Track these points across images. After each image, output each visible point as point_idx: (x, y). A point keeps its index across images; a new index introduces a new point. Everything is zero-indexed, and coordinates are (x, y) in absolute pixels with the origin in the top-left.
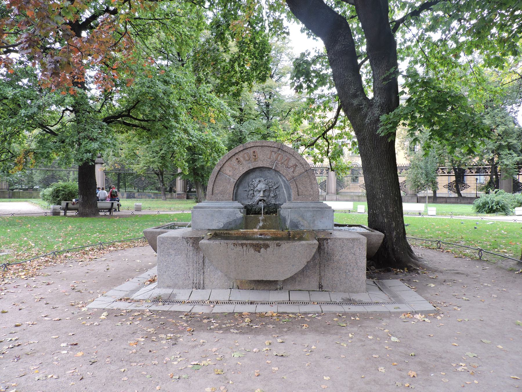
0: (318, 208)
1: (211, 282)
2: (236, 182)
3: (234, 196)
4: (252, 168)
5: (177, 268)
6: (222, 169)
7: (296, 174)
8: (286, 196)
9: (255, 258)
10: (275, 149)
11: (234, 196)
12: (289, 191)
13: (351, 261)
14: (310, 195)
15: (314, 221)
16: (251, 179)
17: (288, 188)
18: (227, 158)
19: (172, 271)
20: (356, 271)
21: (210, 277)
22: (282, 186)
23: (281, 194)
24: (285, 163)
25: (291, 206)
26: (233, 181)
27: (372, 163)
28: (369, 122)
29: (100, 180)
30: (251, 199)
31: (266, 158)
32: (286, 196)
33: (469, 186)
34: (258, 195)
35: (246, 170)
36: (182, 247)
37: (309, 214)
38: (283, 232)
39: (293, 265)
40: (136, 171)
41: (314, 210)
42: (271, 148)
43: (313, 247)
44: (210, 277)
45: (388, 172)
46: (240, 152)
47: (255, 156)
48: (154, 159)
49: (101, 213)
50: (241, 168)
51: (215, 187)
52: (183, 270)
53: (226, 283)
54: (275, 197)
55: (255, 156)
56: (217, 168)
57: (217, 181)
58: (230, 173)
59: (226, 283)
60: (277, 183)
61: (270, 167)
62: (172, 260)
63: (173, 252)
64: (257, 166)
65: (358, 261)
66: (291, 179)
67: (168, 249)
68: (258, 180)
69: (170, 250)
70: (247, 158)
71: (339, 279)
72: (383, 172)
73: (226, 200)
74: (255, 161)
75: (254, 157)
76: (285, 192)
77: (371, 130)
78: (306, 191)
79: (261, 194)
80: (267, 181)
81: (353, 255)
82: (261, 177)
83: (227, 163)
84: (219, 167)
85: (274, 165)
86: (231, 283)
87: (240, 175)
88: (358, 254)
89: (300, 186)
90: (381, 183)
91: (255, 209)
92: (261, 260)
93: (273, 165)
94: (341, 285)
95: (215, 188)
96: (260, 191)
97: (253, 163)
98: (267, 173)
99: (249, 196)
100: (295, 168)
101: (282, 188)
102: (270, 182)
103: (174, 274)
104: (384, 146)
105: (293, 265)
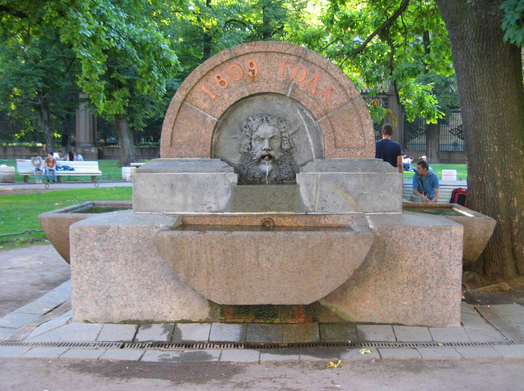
8: (313, 149)
10: (292, 58)
13: (435, 269)
31: (274, 76)
32: (313, 149)
35: (235, 98)
42: (284, 57)
50: (226, 95)
51: (176, 133)
56: (179, 96)
58: (206, 105)
61: (283, 93)
62: (98, 269)
65: (448, 269)
66: (322, 116)
69: (96, 252)
85: (290, 89)
88: (446, 256)
89: (339, 130)
92: (269, 266)
93: (288, 88)
94: (414, 313)
95: (177, 134)
97: (250, 86)
101: (305, 133)
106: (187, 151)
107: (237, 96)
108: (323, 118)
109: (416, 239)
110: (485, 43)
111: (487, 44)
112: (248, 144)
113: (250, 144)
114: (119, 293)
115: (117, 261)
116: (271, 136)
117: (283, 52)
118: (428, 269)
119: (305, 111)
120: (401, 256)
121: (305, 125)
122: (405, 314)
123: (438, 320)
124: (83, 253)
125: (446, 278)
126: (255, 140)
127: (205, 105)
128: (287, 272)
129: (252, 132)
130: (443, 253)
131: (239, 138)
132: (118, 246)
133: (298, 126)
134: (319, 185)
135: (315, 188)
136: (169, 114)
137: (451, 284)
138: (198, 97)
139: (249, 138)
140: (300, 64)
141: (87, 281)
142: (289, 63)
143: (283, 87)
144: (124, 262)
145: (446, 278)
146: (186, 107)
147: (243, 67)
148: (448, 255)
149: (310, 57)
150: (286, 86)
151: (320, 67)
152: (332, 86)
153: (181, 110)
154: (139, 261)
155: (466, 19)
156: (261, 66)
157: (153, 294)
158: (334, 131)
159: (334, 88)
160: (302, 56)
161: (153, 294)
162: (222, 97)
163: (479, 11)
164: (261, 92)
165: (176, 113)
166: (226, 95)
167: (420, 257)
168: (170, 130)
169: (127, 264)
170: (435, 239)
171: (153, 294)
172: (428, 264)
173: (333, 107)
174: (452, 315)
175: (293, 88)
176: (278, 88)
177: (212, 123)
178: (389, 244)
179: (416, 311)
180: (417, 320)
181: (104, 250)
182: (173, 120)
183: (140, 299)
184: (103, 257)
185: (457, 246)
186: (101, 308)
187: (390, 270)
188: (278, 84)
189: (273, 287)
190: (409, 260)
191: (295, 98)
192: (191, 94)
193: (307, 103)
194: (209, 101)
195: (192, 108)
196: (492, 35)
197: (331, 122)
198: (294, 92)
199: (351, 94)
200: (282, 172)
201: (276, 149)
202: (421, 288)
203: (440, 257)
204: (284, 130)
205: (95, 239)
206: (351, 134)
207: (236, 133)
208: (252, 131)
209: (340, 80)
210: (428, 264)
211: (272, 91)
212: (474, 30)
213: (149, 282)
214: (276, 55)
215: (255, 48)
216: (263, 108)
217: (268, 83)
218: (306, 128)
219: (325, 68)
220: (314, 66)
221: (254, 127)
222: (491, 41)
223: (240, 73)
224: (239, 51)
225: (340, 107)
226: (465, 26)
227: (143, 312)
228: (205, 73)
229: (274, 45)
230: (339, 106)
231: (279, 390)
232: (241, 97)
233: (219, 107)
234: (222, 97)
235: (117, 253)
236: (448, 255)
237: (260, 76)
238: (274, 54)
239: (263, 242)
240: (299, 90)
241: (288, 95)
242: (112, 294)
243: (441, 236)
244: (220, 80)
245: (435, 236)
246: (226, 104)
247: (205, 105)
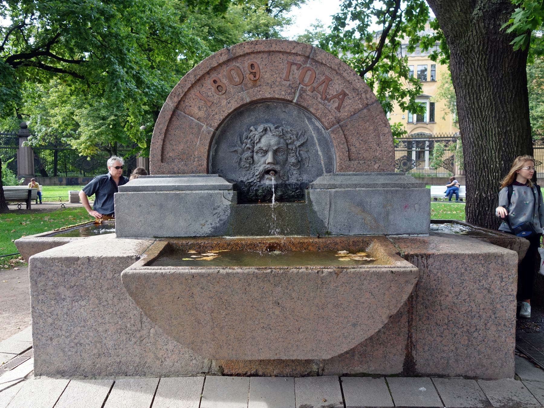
0: (396, 185)
1: (158, 359)
2: (214, 134)
3: (210, 164)
4: (248, 100)
5: (79, 329)
6: (183, 105)
7: (344, 114)
8: (322, 162)
9: (261, 309)
10: (299, 58)
11: (210, 164)
12: (329, 151)
13: (482, 306)
14: (376, 159)
15: (387, 215)
16: (245, 127)
17: (326, 144)
18: (192, 79)
19: (67, 337)
20: (493, 328)
21: (157, 349)
22: (313, 140)
23: (312, 159)
24: (321, 89)
25: (335, 182)
26: (207, 130)
27: (484, 98)
28: (481, 14)
29: (27, 160)
30: (248, 169)
31: (278, 79)
32: (322, 162)
33: (541, 163)
34: (263, 160)
35: (234, 105)
36: (89, 281)
37: (376, 201)
38: (320, 240)
39: (354, 325)
40: (76, 148)
41: (387, 192)
42: (290, 57)
43: (407, 282)
44: (157, 349)
45: (516, 116)
46: (220, 65)
47: (254, 74)
48: (99, 130)
49: (12, 207)
50: (224, 102)
51: (168, 145)
52: (91, 334)
53: (194, 361)
54: (300, 163)
55: (254, 74)
56: (170, 103)
57: (172, 132)
58: (201, 114)
59: (194, 361)
60: (303, 134)
61: (289, 98)
62: (65, 310)
63: (68, 293)
64: (259, 97)
65: (498, 306)
66: (333, 125)
67: (56, 286)
68: (260, 128)
69: (61, 289)
70: (237, 80)
71: (453, 348)
72: (505, 116)
73: (193, 172)
74: (254, 86)
75: (252, 76)
76: (320, 153)
77: (484, 31)
78: (367, 150)
79: (269, 158)
80: (280, 129)
81: (485, 292)
82: (267, 121)
83: (192, 92)
84: (176, 100)
85: (297, 94)
86: (206, 361)
87: (222, 118)
88: (497, 291)
89: (353, 140)
90: (500, 139)
91: (257, 190)
92: (277, 312)
93: (295, 93)
94: (457, 361)
95: (168, 146)
96: (266, 152)
97: (251, 91)
98: (281, 113)
99: (242, 163)
100: (342, 101)
101: (314, 145)
102: (287, 132)
103: (73, 344)
104: (509, 64)
105: (354, 325)
106: (180, 166)
107: (236, 103)
108: (335, 126)
109: (458, 269)
110: (493, 55)
111: (494, 57)
112: (249, 158)
113: (252, 157)
114: (90, 339)
115: (89, 300)
116: (275, 148)
117: (289, 51)
118: (474, 306)
119: (313, 120)
120: (440, 291)
121: (314, 135)
122: (446, 362)
123: (487, 370)
124: (45, 290)
125: (496, 318)
126: (257, 152)
127: (200, 113)
128: (302, 319)
129: (253, 145)
130: (492, 287)
131: (239, 152)
132: (89, 281)
133: (306, 136)
134: (333, 203)
135: (328, 206)
136: (159, 124)
137: (502, 325)
139: (250, 151)
140: (308, 65)
141: (51, 324)
142: (296, 64)
143: (289, 91)
144: (97, 302)
145: (496, 318)
146: (179, 116)
147: (242, 70)
148: (499, 289)
149: (319, 57)
150: (293, 91)
151: (331, 67)
152: (345, 90)
153: (173, 119)
154: (115, 300)
155: (472, 31)
156: (263, 68)
157: (133, 340)
158: (347, 142)
159: (347, 92)
160: (311, 56)
161: (133, 339)
162: (219, 104)
163: (487, 21)
164: (264, 97)
165: (166, 124)
166: (224, 102)
167: (464, 291)
168: (160, 142)
169: (100, 304)
170: (483, 269)
171: (133, 339)
172: (474, 300)
173: (346, 114)
174: (505, 364)
175: (300, 93)
176: (283, 93)
177: (209, 133)
178: (425, 276)
179: (460, 358)
180: (460, 369)
181: (71, 287)
182: (164, 130)
183: (117, 347)
184: (71, 295)
185: (510, 277)
186: (69, 359)
187: (426, 308)
188: (284, 88)
189: (282, 338)
190: (450, 295)
191: (303, 104)
192: (184, 101)
193: (317, 110)
194: (205, 109)
195: (185, 117)
196: (501, 47)
197: (343, 132)
198: (302, 98)
199: (367, 99)
200: (288, 189)
201: (282, 163)
202: (465, 330)
203: (489, 291)
204: (290, 141)
205: (60, 273)
206: (366, 145)
207: (235, 146)
208: (254, 143)
209: (353, 83)
210: (474, 300)
212: (480, 42)
213: (128, 325)
214: (281, 55)
215: (257, 47)
216: (266, 117)
218: (315, 139)
219: (337, 68)
220: (324, 67)
221: (255, 138)
222: (499, 53)
223: (239, 76)
224: (238, 50)
225: (354, 114)
226: (471, 38)
227: (120, 361)
228: (199, 76)
230: (352, 113)
232: (241, 104)
233: (216, 116)
234: (219, 104)
235: (89, 290)
236: (499, 289)
237: (262, 80)
238: (278, 54)
239: (269, 281)
240: (307, 95)
241: (295, 101)
242: (82, 341)
243: (490, 266)
244: (217, 85)
246: (224, 111)
247: (200, 113)
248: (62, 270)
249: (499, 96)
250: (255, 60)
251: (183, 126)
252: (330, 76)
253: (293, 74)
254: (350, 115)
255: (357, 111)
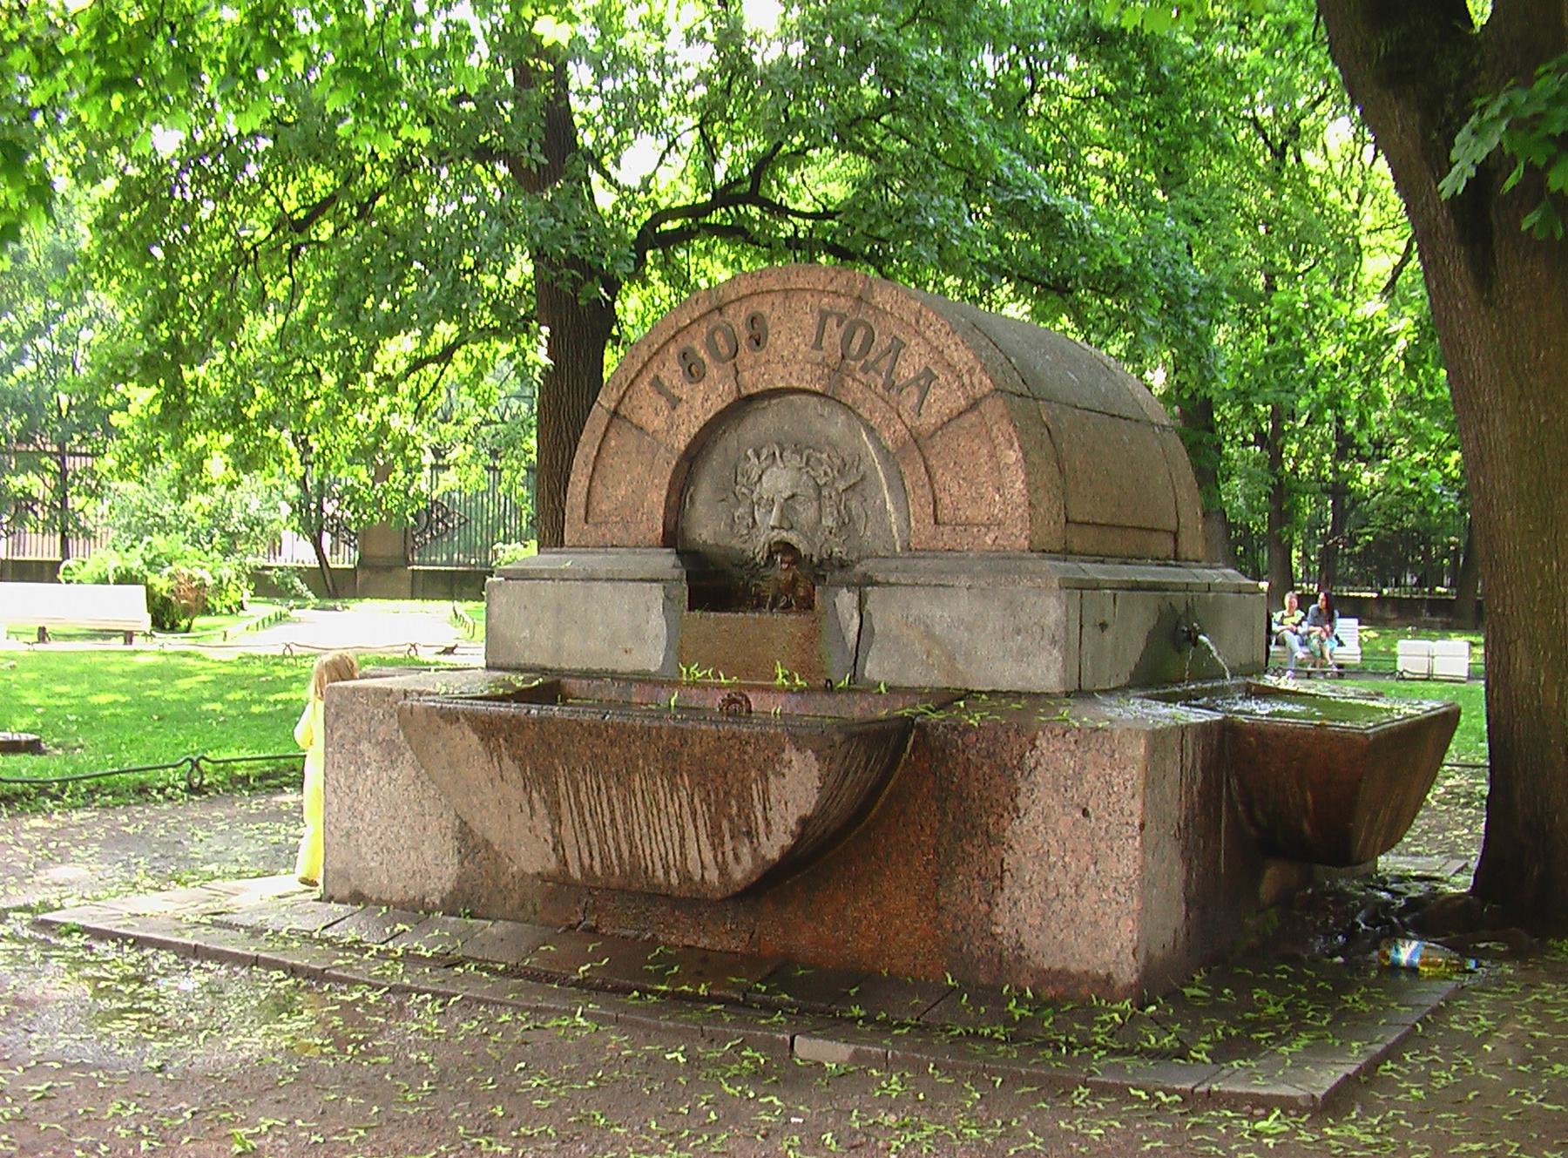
7: (929, 420)
89: (944, 478)
100: (924, 393)
125: (1098, 872)
137: (1111, 890)
138: (643, 403)
190: (1006, 814)
197: (925, 461)
203: (1085, 813)
211: (795, 384)
217: (785, 365)
229: (801, 273)
231: (3, 430)
245: (1073, 754)
248: (367, 711)
249: (1508, 353)
250: (760, 310)
251: (627, 449)
252: (902, 336)
253: (830, 337)
254: (940, 422)
255: (955, 413)
